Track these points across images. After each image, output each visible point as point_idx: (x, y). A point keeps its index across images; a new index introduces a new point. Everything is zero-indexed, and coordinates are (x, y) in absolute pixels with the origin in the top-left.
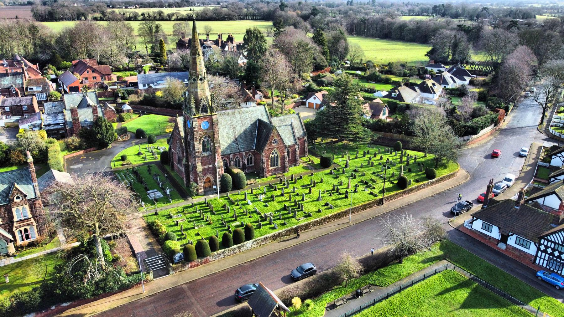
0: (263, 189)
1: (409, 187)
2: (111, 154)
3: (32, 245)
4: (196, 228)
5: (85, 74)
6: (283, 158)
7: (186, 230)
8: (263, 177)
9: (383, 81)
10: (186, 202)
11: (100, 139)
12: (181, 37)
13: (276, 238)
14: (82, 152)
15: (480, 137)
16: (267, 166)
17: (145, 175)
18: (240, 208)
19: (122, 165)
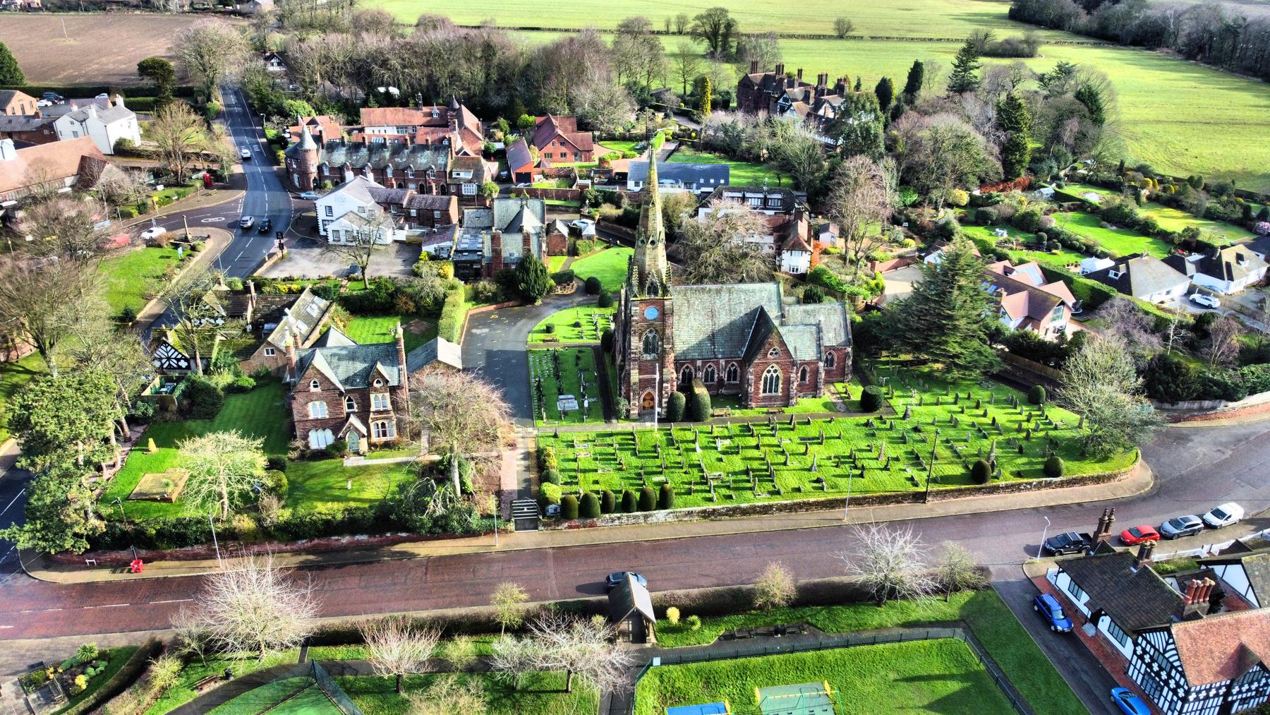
0: (735, 428)
1: (990, 484)
2: (537, 316)
3: (387, 445)
4: (600, 472)
5: (549, 148)
6: (788, 382)
7: (585, 471)
8: (746, 408)
9: (1137, 227)
10: (605, 425)
11: (524, 290)
12: (748, 71)
13: (709, 516)
14: (492, 307)
15: (1251, 406)
16: (756, 389)
17: (569, 366)
18: (680, 455)
19: (544, 341)
